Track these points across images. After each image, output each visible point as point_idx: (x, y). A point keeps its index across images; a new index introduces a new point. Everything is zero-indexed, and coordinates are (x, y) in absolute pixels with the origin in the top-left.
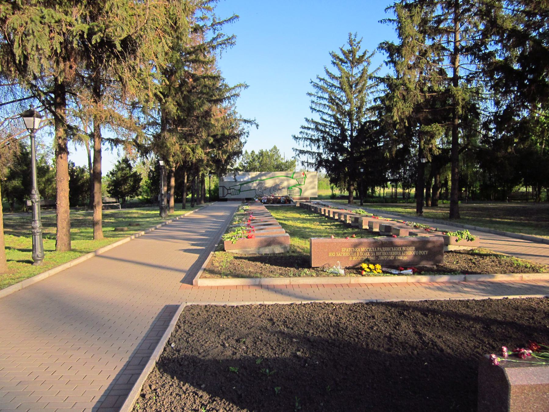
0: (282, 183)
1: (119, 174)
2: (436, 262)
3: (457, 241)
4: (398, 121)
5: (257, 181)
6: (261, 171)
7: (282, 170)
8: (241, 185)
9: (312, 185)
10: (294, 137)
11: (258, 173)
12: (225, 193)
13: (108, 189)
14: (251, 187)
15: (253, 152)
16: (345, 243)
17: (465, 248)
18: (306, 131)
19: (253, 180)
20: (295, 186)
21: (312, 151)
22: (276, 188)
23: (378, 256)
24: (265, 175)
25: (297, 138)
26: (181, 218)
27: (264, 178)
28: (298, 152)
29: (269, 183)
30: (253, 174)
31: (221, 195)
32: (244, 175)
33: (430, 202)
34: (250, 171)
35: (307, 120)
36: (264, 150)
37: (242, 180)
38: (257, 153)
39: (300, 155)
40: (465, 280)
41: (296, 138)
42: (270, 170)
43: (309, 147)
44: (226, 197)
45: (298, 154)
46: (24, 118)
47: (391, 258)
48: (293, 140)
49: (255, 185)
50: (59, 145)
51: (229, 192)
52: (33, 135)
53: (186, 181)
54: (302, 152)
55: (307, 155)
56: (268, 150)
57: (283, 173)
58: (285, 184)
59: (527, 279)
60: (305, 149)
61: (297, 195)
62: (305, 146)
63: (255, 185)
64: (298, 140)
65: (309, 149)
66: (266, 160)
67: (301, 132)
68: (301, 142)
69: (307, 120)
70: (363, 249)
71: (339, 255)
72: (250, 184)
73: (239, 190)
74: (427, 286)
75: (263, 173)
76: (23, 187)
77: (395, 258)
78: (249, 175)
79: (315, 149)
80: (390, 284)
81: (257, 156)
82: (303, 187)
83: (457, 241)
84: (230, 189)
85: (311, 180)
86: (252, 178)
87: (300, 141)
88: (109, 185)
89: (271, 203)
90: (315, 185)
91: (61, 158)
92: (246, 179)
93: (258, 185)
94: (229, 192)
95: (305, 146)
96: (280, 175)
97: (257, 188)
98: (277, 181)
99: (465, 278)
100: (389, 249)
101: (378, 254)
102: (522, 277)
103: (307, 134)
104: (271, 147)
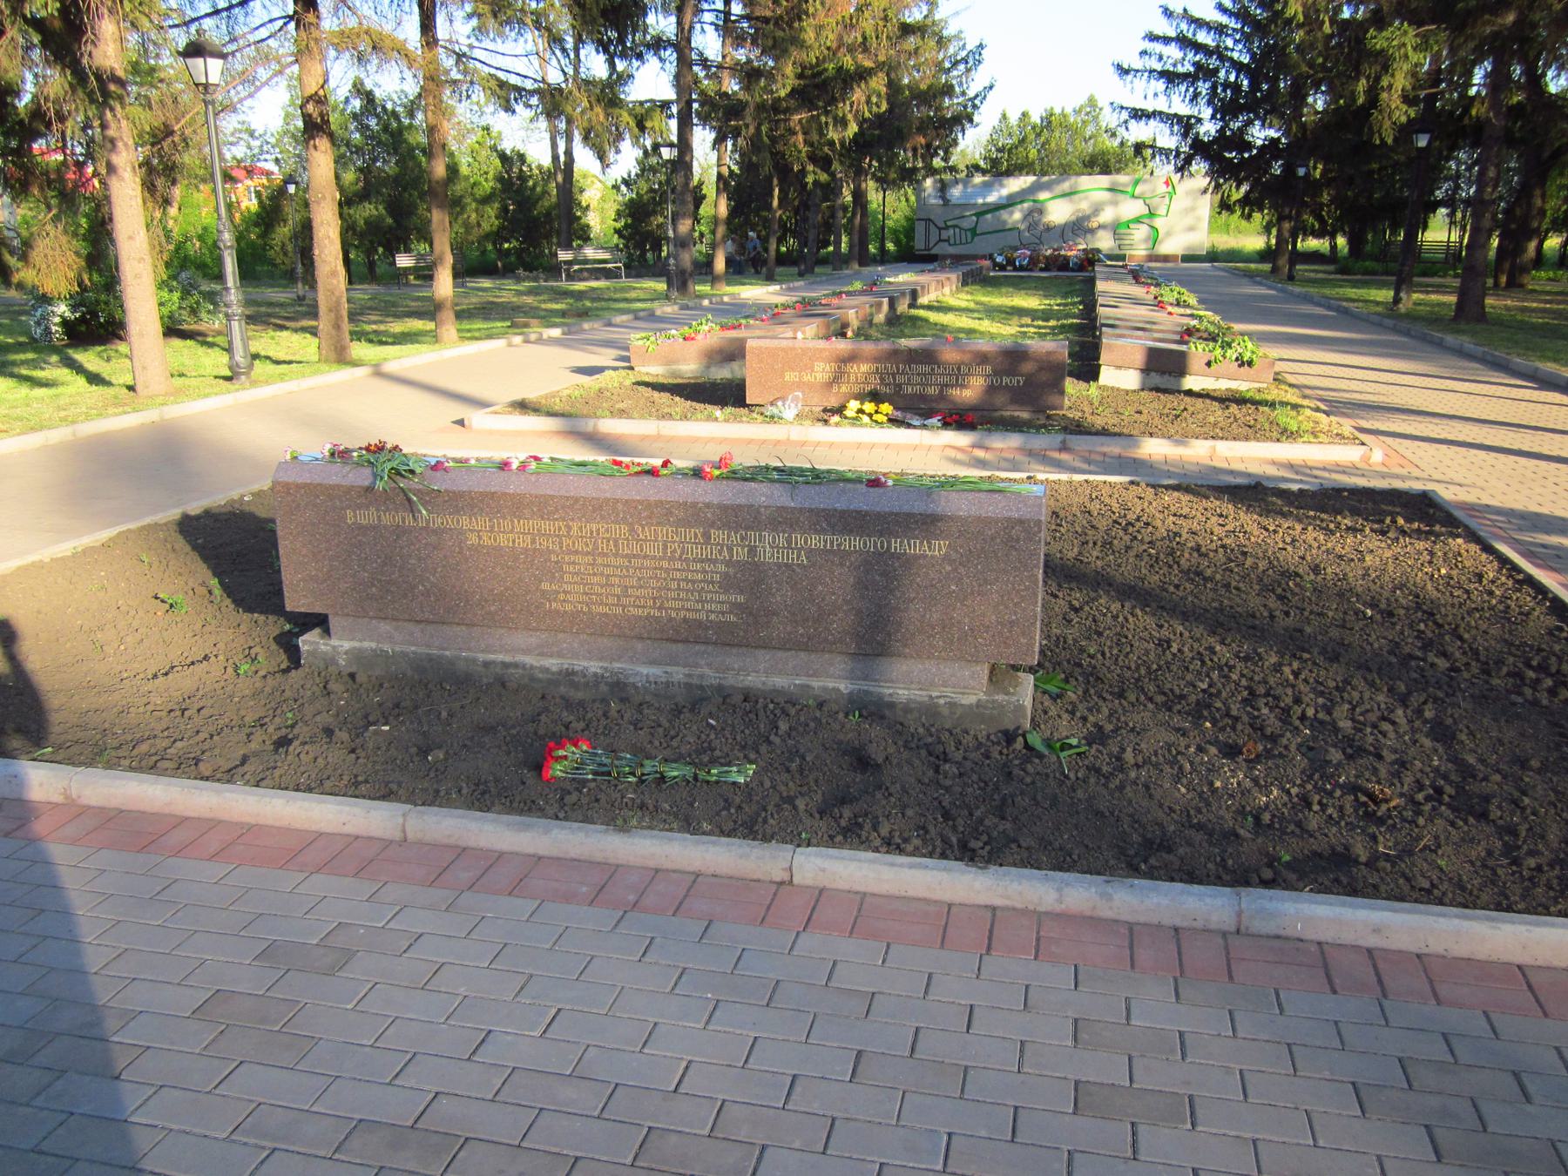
0: (1097, 210)
1: (644, 186)
2: (1040, 410)
3: (1209, 364)
4: (1301, 18)
5: (1026, 205)
6: (1044, 173)
7: (1106, 170)
8: (979, 215)
9: (1189, 221)
10: (1119, 67)
11: (1031, 179)
12: (934, 239)
13: (618, 225)
14: (1005, 222)
15: (1024, 114)
16: (821, 350)
17: (1234, 385)
18: (1158, 47)
19: (1010, 202)
20: (1138, 220)
21: (1172, 111)
22: (1079, 227)
23: (900, 386)
24: (1047, 187)
25: (1127, 72)
26: (723, 303)
27: (1043, 196)
28: (1125, 115)
29: (1058, 212)
30: (1015, 184)
31: (919, 244)
32: (987, 187)
33: (1503, 279)
34: (1009, 173)
35: (1168, 13)
36: (1057, 111)
37: (980, 201)
38: (1035, 118)
39: (1133, 123)
40: (1064, 448)
41: (1123, 71)
42: (1066, 171)
43: (1162, 98)
44: (933, 252)
45: (1126, 122)
46: (189, 61)
47: (932, 391)
48: (1116, 77)
49: (1017, 216)
50: (307, 118)
51: (945, 235)
52: (209, 98)
53: (775, 203)
54: (1138, 115)
55: (1152, 122)
56: (1069, 110)
57: (1104, 180)
58: (1106, 216)
59: (1228, 454)
60: (1150, 106)
61: (1143, 246)
62: (1150, 96)
63: (1017, 216)
64: (1130, 77)
65: (1161, 105)
66: (1058, 139)
67: (1144, 53)
68: (1140, 83)
69: (1168, 13)
70: (864, 368)
71: (807, 378)
72: (1004, 215)
73: (973, 231)
74: (960, 456)
75: (1046, 179)
76: (389, 221)
77: (941, 391)
78: (1002, 186)
79: (1181, 107)
80: (859, 445)
81: (1034, 128)
82: (1158, 222)
83: (1209, 364)
84: (947, 228)
85: (1188, 203)
86: (1010, 197)
87: (1136, 81)
88: (619, 214)
89: (1042, 270)
90: (1199, 219)
91: (315, 147)
92: (992, 198)
93: (1025, 218)
94: (945, 235)
95: (1150, 96)
96: (1093, 186)
97: (1022, 227)
98: (1084, 206)
99: (1064, 442)
100: (927, 369)
101: (900, 379)
102: (1214, 448)
103: (1161, 58)
104: (1082, 100)
